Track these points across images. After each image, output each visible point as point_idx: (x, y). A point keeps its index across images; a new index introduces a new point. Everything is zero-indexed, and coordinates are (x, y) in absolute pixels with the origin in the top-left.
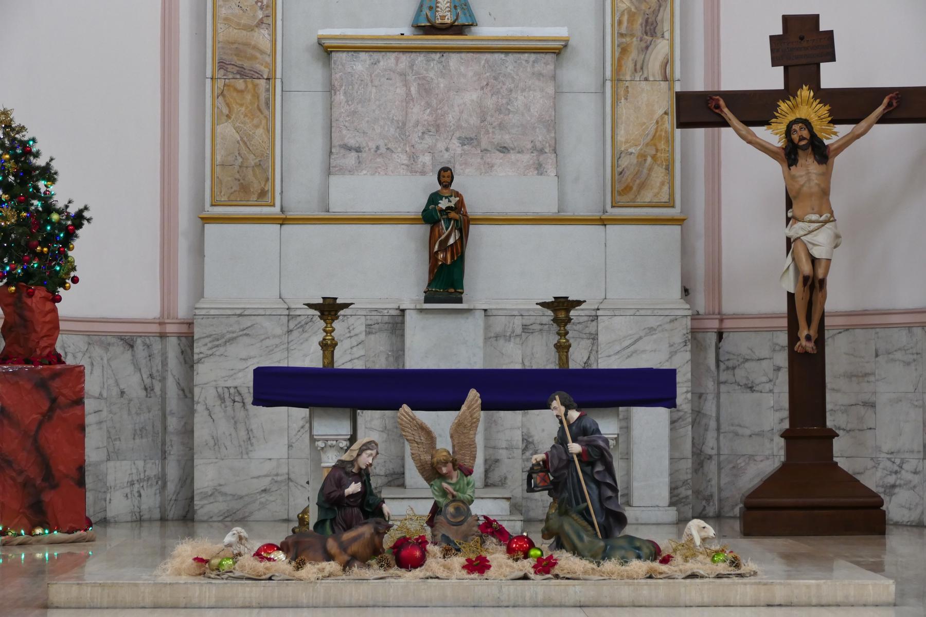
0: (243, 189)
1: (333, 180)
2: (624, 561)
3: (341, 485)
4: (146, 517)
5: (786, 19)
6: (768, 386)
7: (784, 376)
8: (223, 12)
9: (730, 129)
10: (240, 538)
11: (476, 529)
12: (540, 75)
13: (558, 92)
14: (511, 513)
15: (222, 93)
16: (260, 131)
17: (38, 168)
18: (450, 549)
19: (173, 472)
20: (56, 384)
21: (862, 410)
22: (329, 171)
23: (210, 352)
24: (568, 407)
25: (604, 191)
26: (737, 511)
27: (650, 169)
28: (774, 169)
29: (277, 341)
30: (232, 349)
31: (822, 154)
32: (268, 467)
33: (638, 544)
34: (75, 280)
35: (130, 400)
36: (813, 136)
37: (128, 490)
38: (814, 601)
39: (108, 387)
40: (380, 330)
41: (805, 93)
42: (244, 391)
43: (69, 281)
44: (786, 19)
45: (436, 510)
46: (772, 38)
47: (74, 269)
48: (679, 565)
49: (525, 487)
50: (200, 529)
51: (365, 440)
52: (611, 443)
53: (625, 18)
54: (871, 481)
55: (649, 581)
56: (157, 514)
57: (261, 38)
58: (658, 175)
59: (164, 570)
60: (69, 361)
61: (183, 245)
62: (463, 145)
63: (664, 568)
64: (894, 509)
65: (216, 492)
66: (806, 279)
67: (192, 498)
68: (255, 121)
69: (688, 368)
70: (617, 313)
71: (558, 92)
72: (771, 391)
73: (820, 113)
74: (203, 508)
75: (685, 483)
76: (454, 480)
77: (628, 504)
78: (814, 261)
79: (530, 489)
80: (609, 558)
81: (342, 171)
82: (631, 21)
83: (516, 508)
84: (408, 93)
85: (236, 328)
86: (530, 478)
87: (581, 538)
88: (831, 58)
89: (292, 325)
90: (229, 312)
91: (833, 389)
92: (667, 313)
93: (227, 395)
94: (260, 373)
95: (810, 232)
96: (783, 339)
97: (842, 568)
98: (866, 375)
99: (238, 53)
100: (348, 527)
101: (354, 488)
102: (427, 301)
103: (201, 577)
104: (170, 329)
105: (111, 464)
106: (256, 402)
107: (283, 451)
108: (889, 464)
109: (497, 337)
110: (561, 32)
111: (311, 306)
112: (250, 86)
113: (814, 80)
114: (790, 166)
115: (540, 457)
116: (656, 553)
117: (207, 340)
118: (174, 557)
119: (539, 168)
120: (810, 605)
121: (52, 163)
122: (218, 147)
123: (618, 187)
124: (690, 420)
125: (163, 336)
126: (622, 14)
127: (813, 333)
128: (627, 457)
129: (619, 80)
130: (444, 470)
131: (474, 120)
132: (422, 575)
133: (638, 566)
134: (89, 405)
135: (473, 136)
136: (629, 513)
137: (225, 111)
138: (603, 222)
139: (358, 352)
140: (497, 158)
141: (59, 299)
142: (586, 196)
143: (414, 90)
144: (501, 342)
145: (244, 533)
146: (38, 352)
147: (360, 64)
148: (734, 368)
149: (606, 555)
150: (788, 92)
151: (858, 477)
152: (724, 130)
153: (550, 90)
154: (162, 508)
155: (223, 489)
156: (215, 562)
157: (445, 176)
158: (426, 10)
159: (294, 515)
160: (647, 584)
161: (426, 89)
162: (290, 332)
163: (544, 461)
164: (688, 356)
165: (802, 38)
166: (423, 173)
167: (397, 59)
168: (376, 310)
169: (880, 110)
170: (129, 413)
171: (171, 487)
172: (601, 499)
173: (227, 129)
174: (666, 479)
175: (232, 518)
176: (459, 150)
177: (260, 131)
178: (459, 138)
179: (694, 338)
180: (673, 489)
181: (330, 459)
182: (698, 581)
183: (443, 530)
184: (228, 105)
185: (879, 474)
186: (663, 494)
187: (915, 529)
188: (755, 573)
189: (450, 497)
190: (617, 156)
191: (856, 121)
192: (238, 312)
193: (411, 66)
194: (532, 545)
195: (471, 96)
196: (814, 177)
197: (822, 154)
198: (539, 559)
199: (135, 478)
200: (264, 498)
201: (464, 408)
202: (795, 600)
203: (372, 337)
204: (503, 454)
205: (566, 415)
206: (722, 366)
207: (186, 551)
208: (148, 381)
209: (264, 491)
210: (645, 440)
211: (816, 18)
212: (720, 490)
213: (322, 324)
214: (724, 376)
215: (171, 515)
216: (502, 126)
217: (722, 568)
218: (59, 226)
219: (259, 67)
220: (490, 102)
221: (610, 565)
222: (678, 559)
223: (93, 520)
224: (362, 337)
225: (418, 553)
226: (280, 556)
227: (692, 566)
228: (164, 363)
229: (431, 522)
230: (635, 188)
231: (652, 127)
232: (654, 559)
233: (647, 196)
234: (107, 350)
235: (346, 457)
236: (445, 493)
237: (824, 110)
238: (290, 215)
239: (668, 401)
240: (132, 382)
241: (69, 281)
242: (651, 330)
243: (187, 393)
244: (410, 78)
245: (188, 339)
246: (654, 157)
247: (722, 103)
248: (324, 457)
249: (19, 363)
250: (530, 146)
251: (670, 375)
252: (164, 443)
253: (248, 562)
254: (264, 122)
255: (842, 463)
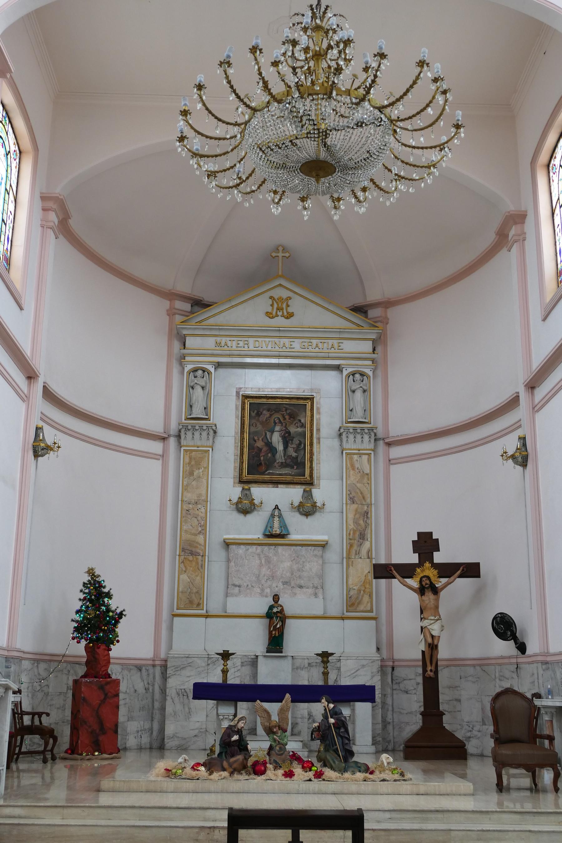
0: (190, 602)
1: (229, 599)
2: (354, 773)
3: (230, 736)
4: (143, 747)
5: (419, 534)
6: (414, 692)
7: (421, 687)
8: (185, 527)
9: (396, 580)
10: (185, 760)
11: (288, 757)
12: (316, 556)
13: (324, 563)
14: (303, 748)
15: (183, 562)
16: (198, 578)
17: (105, 593)
18: (277, 767)
19: (156, 726)
20: (107, 687)
21: (455, 702)
22: (227, 595)
23: (174, 673)
24: (329, 703)
25: (343, 603)
26: (402, 748)
27: (363, 596)
28: (415, 596)
29: (203, 669)
30: (183, 672)
31: (435, 591)
32: (197, 725)
33: (359, 765)
34: (118, 641)
35: (139, 694)
36: (431, 583)
37: (136, 735)
38: (437, 793)
39: (129, 686)
40: (247, 665)
41: (427, 565)
42: (188, 691)
43: (115, 642)
44: (419, 534)
45: (271, 748)
46: (413, 541)
47: (118, 636)
48: (377, 775)
49: (310, 738)
50: (167, 753)
51: (241, 716)
52: (347, 718)
53: (352, 532)
54: (460, 735)
55: (365, 782)
56: (148, 746)
57: (200, 539)
58: (366, 598)
59: (152, 774)
60: (114, 677)
61: (164, 626)
62: (284, 585)
63: (371, 776)
64: (471, 748)
65: (174, 736)
66: (429, 645)
67: (164, 739)
68: (197, 573)
69: (380, 683)
70: (349, 658)
71: (324, 563)
72: (415, 694)
73: (434, 573)
74: (169, 743)
75: (379, 734)
76: (279, 734)
77: (354, 744)
78: (433, 637)
79: (312, 739)
80: (347, 772)
81: (233, 595)
82: (354, 534)
83: (305, 745)
84: (261, 563)
85: (185, 663)
86: (312, 734)
87: (334, 762)
88: (438, 550)
89: (209, 662)
90: (183, 656)
91: (442, 693)
92: (370, 658)
93: (180, 693)
94: (196, 685)
95: (431, 624)
96: (420, 670)
97: (448, 776)
98: (456, 687)
99: (190, 545)
100: (233, 756)
101: (236, 738)
102: (267, 652)
103: (168, 778)
104: (157, 663)
105: (129, 723)
106: (195, 698)
107: (203, 718)
108: (467, 727)
109: (297, 668)
110: (325, 538)
111: (218, 654)
112: (195, 559)
113: (431, 559)
114: (421, 596)
115: (316, 725)
116: (367, 769)
117: (173, 668)
118: (156, 768)
119: (316, 595)
120: (436, 795)
121: (111, 591)
122: (181, 584)
123: (350, 604)
124: (380, 706)
125: (154, 666)
126: (351, 530)
127: (433, 669)
128: (354, 723)
129: (349, 558)
130: (275, 730)
131: (288, 574)
132: (264, 778)
133: (360, 775)
134: (121, 696)
135: (288, 581)
136: (355, 749)
137: (184, 569)
138: (343, 618)
139: (238, 674)
140: (298, 590)
141: (111, 650)
142: (336, 608)
143: (263, 561)
144: (299, 670)
145: (187, 758)
146: (101, 673)
147: (241, 550)
148: (399, 683)
149: (345, 770)
150: (421, 564)
151: (454, 733)
152: (393, 580)
153: (320, 562)
154: (151, 744)
155: (178, 735)
156: (174, 771)
157: (276, 598)
158: (269, 528)
159: (208, 747)
160: (363, 784)
161: (268, 561)
162: (208, 665)
163: (318, 726)
164: (379, 678)
165: (425, 542)
166: (266, 596)
167: (256, 549)
168: (245, 656)
169: (459, 572)
170: (138, 700)
171: (155, 733)
172: (343, 744)
173: (184, 577)
174: (370, 733)
175: (182, 749)
176: (282, 587)
177: (198, 578)
178: (282, 582)
179: (382, 670)
180: (374, 738)
181: (225, 724)
182: (386, 782)
183: (274, 758)
184: (185, 567)
185: (463, 731)
186: (369, 739)
187: (480, 758)
188: (411, 779)
189: (277, 742)
190: (349, 590)
191: (449, 577)
192: (187, 656)
193: (262, 552)
194: (313, 765)
195: (287, 564)
196: (432, 600)
197: (435, 591)
198: (316, 771)
199: (139, 729)
200: (196, 738)
201: (284, 702)
202: (429, 792)
203: (244, 667)
204: (299, 720)
205: (328, 706)
206: (394, 682)
207: (161, 765)
208: (147, 686)
209: (195, 736)
210: (361, 716)
211: (431, 534)
212: (394, 738)
213: (222, 662)
214: (395, 687)
215: (154, 746)
216: (300, 577)
217: (397, 777)
218: (112, 618)
219: (198, 551)
220: (295, 567)
221: (347, 775)
222: (377, 772)
223: (120, 748)
224: (239, 667)
225: (263, 768)
226: (202, 768)
227: (383, 776)
228: (154, 677)
229: (269, 754)
230: (356, 604)
231: (363, 578)
232: (366, 773)
233: (362, 607)
234: (130, 671)
235: (232, 724)
236: (275, 740)
237: (436, 572)
238: (210, 614)
239: (372, 699)
240: (140, 686)
241: (115, 642)
242: (363, 666)
243: (163, 691)
244: (262, 556)
245: (165, 667)
246: (364, 591)
247: (393, 569)
248: (223, 723)
249: (92, 678)
250: (312, 586)
251: (373, 688)
252: (152, 713)
253: (188, 771)
254: (200, 574)
255: (447, 727)
